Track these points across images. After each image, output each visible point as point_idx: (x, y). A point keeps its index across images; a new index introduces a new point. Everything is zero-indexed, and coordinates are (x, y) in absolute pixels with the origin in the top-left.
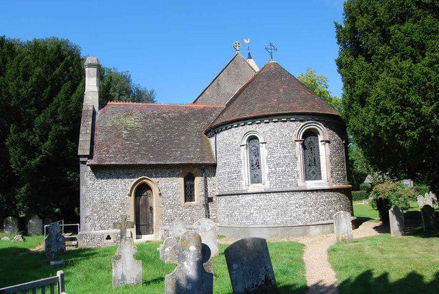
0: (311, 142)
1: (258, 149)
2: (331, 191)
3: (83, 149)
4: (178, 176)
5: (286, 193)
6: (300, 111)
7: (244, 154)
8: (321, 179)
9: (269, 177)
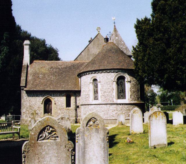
0: (121, 82)
1: (97, 85)
2: (130, 105)
3: (23, 84)
4: (63, 96)
5: (108, 105)
6: (115, 68)
7: (91, 87)
8: (125, 98)
9: (101, 97)
